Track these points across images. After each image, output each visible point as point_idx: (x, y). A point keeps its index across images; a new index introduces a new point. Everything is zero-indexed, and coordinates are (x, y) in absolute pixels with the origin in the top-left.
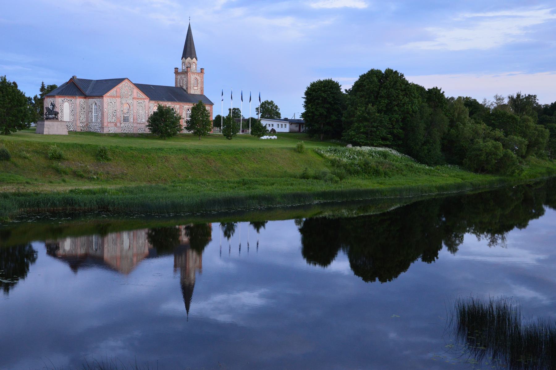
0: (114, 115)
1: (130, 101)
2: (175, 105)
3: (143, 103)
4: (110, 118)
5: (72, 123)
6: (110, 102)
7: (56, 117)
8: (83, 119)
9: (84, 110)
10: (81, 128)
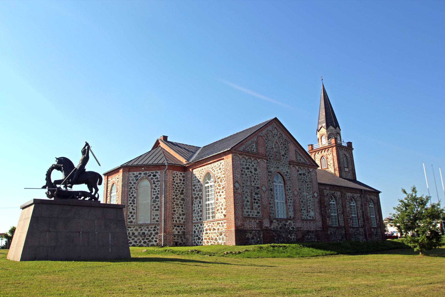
0: (255, 199)
1: (284, 169)
2: (336, 193)
3: (307, 174)
4: (247, 206)
5: (155, 227)
6: (245, 167)
7: (92, 191)
8: (181, 217)
9: (182, 196)
10: (176, 238)
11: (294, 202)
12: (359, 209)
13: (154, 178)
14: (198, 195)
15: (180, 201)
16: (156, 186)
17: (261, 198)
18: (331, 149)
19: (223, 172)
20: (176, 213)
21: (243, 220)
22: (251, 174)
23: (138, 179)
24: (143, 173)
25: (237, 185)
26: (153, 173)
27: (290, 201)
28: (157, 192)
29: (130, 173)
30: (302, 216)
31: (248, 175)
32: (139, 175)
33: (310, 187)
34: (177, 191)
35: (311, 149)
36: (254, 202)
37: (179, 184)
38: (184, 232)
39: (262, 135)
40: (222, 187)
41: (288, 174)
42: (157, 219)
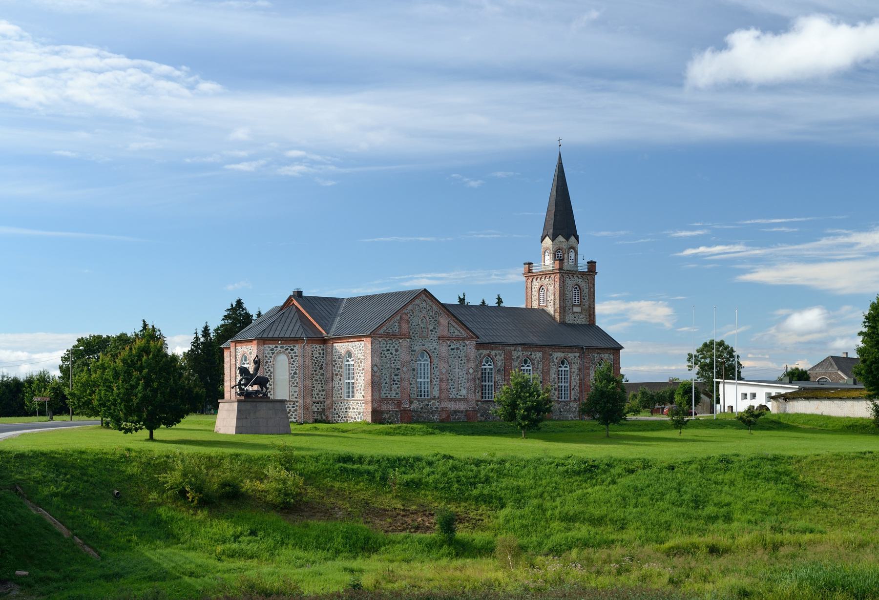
0: (394, 381)
1: (430, 347)
3: (461, 348)
4: (385, 387)
5: (294, 404)
6: (385, 349)
7: (262, 390)
8: (320, 393)
9: (322, 371)
10: (315, 415)
11: (441, 381)
12: (575, 375)
13: (292, 352)
14: (339, 371)
15: (319, 376)
16: (294, 361)
17: (401, 379)
18: (553, 276)
19: (363, 354)
20: (315, 389)
21: (380, 401)
22: (391, 356)
23: (274, 353)
24: (279, 346)
25: (375, 369)
26: (290, 347)
27: (436, 379)
28: (296, 368)
29: (265, 346)
30: (450, 395)
31: (387, 357)
32: (275, 349)
33: (464, 363)
34: (317, 366)
35: (527, 271)
36: (393, 384)
37: (318, 359)
38: (323, 409)
39: (406, 312)
40: (361, 368)
41: (435, 351)
42: (296, 396)
